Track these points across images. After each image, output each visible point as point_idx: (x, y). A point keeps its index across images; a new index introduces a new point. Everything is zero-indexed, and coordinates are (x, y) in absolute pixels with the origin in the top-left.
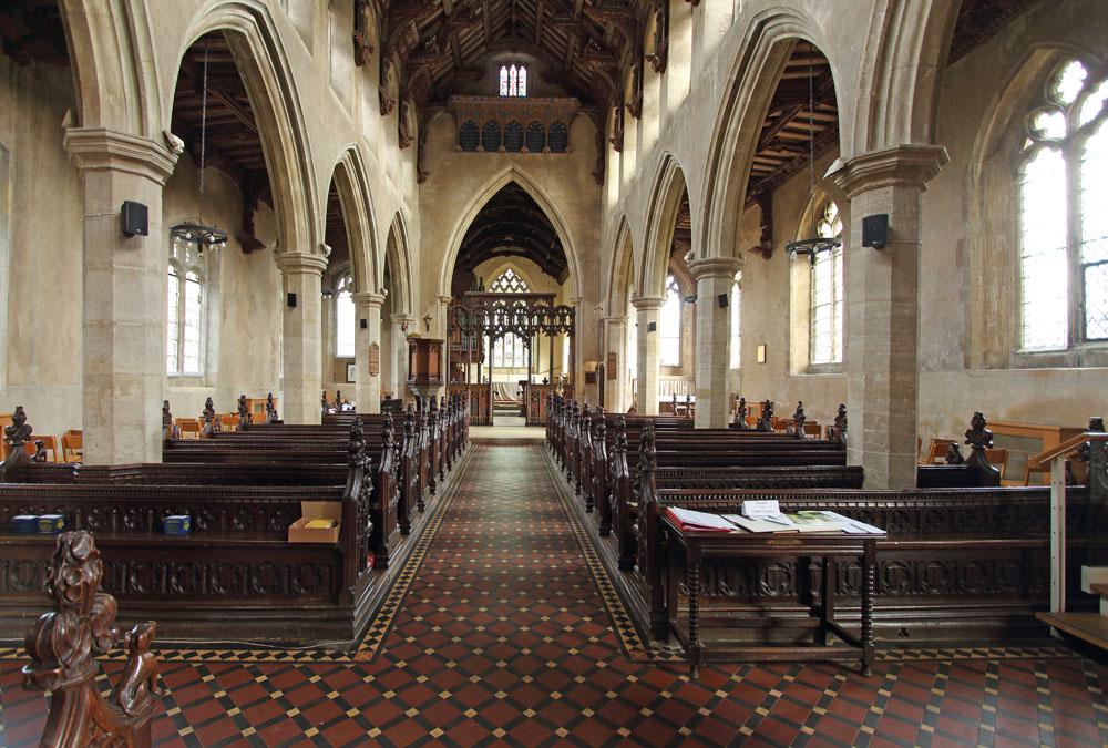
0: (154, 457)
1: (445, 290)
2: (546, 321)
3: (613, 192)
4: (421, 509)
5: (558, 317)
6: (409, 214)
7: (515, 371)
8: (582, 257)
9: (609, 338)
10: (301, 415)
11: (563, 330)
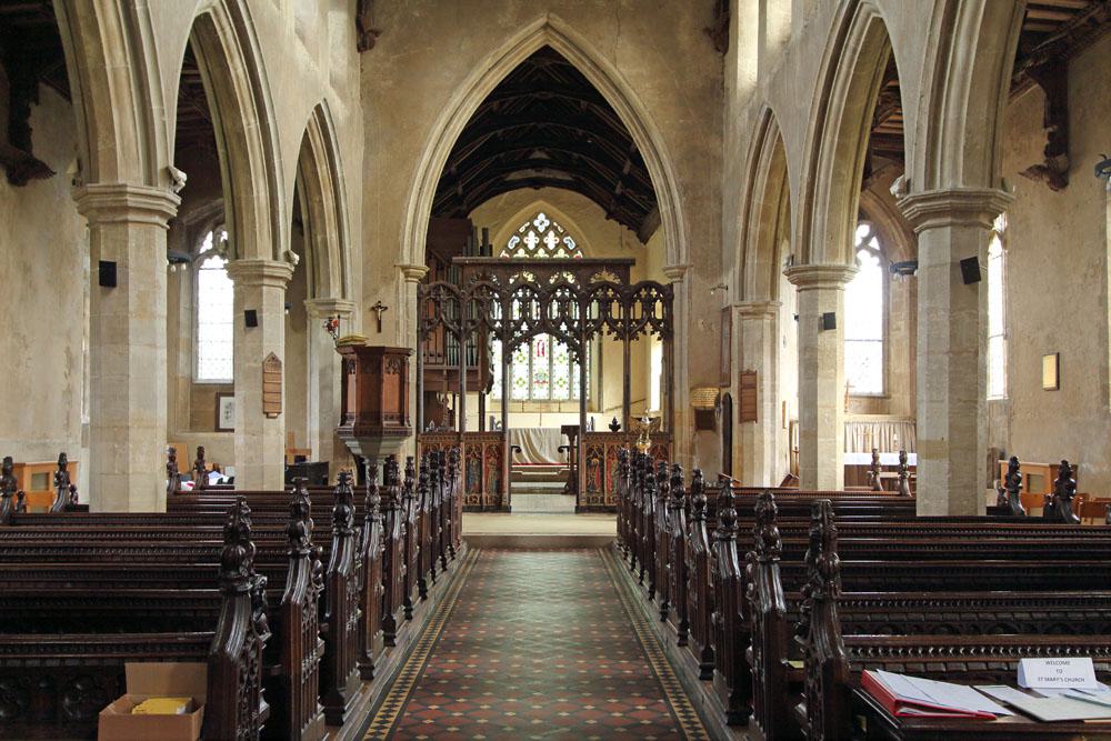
0: (163, 509)
2: (616, 311)
3: (747, 65)
5: (638, 305)
7: (555, 407)
8: (685, 189)
9: (741, 344)
11: (649, 328)
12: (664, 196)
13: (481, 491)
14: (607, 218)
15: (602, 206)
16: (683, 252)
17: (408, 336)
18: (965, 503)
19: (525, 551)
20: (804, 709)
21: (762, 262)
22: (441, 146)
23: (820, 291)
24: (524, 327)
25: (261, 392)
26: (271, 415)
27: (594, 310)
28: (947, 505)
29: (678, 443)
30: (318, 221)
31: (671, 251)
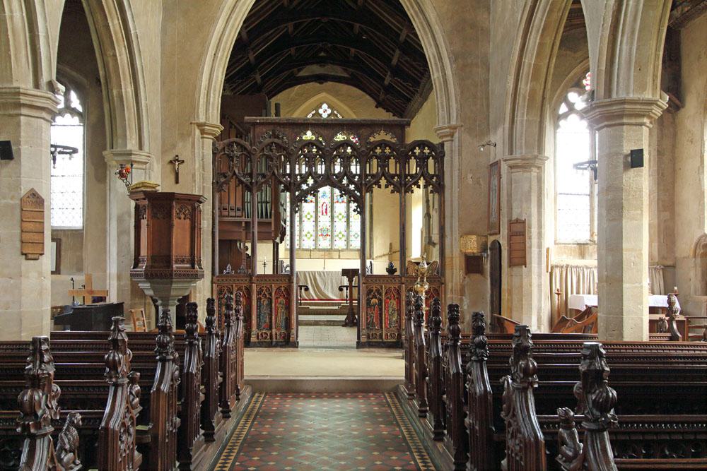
2: (392, 167)
5: (413, 162)
7: (335, 255)
8: (455, 57)
9: (509, 195)
12: (436, 64)
13: (271, 328)
14: (377, 107)
15: (373, 98)
16: (454, 114)
17: (204, 187)
19: (310, 397)
21: (531, 119)
22: (234, 16)
24: (311, 181)
25: (19, 231)
26: (30, 256)
29: (449, 286)
31: (442, 113)
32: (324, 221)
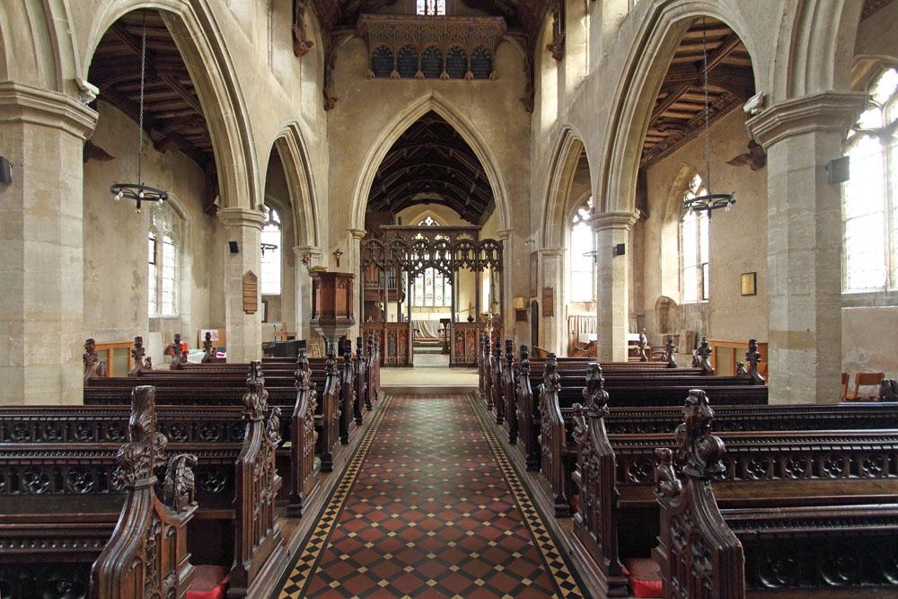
0: (78, 400)
1: (358, 220)
2: (471, 256)
3: (549, 110)
4: (359, 423)
5: (484, 252)
6: (310, 135)
8: (509, 188)
9: (543, 272)
10: (21, 384)
18: (831, 390)
20: (580, 475)
23: (614, 230)
27: (459, 255)
28: (815, 393)
29: (506, 328)
30: (299, 202)
32: (429, 289)
